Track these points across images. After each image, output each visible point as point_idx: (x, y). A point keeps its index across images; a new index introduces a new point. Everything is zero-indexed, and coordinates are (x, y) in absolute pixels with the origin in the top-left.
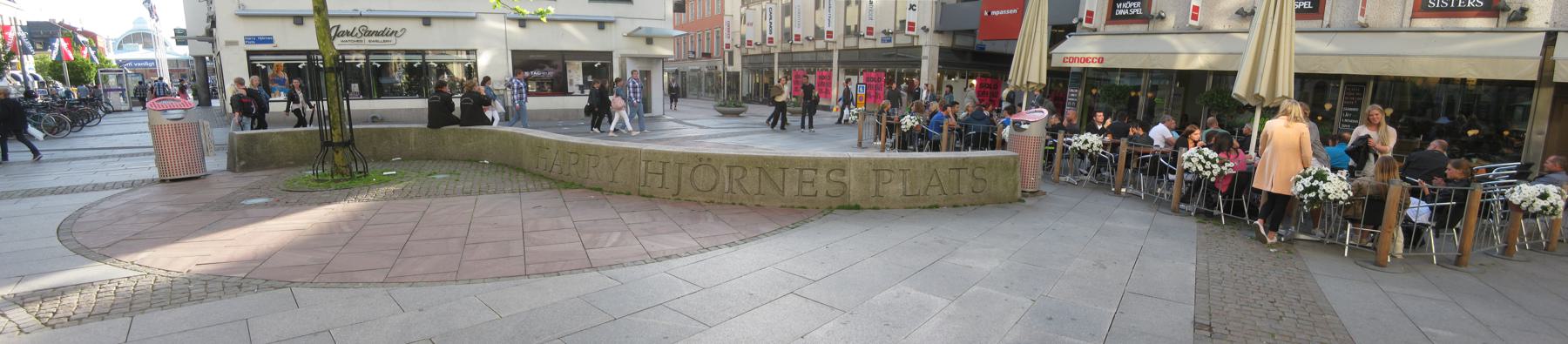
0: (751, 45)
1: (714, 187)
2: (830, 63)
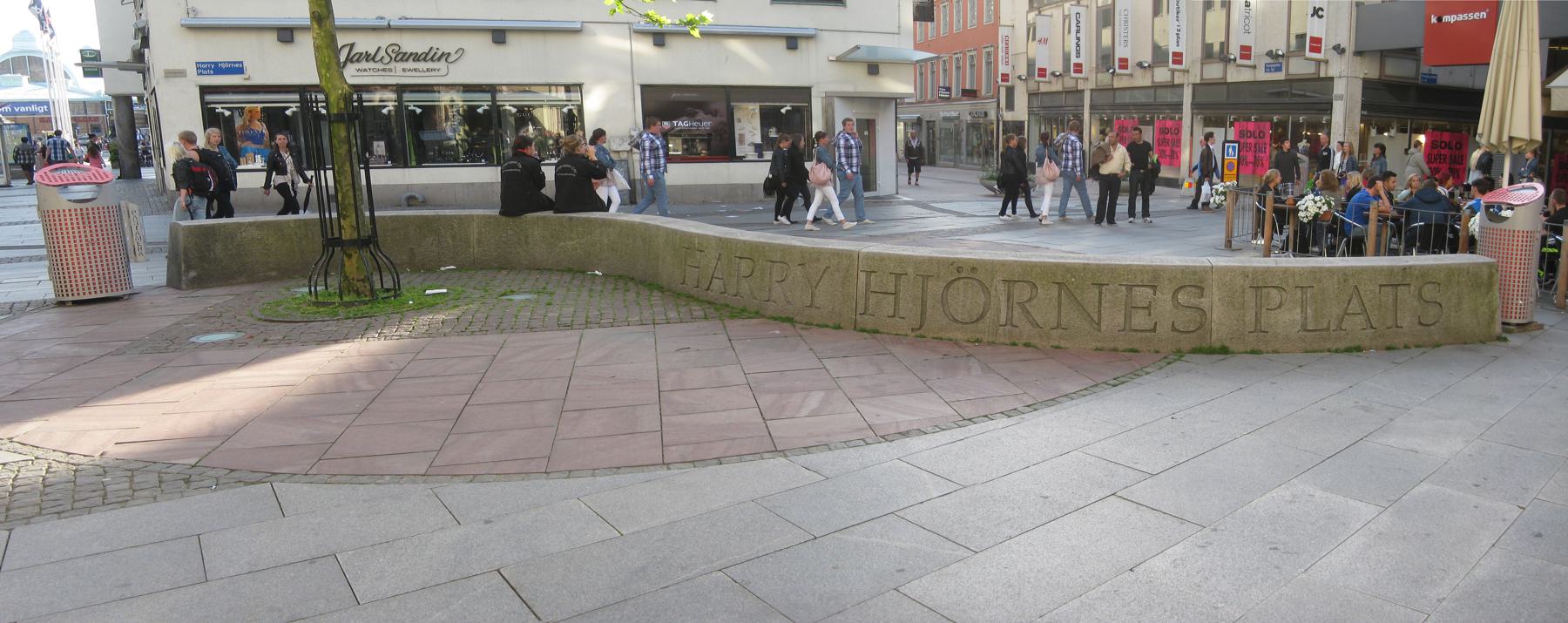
0: (1044, 76)
1: (982, 316)
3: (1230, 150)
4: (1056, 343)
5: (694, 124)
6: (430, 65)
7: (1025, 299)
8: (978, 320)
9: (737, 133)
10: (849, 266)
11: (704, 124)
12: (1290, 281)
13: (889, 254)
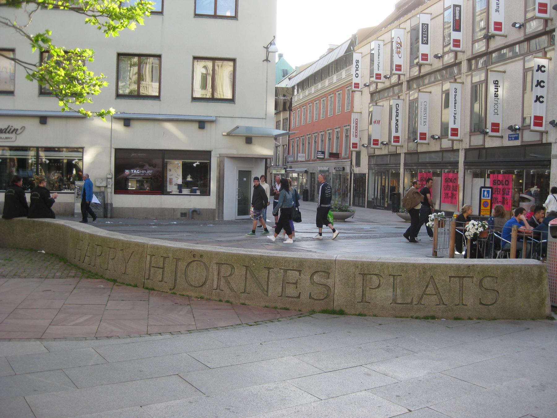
0: (377, 144)
1: (204, 283)
2: (455, 164)
3: (486, 193)
4: (243, 302)
5: (143, 172)
6: (8, 135)
7: (228, 275)
8: (202, 285)
9: (169, 177)
10: (143, 252)
11: (148, 172)
12: (386, 271)
13: (161, 245)
